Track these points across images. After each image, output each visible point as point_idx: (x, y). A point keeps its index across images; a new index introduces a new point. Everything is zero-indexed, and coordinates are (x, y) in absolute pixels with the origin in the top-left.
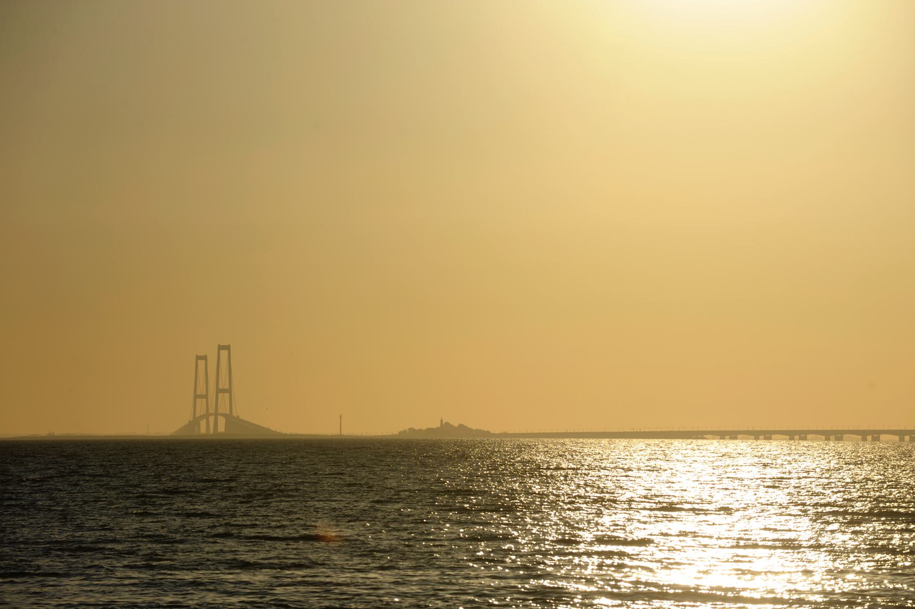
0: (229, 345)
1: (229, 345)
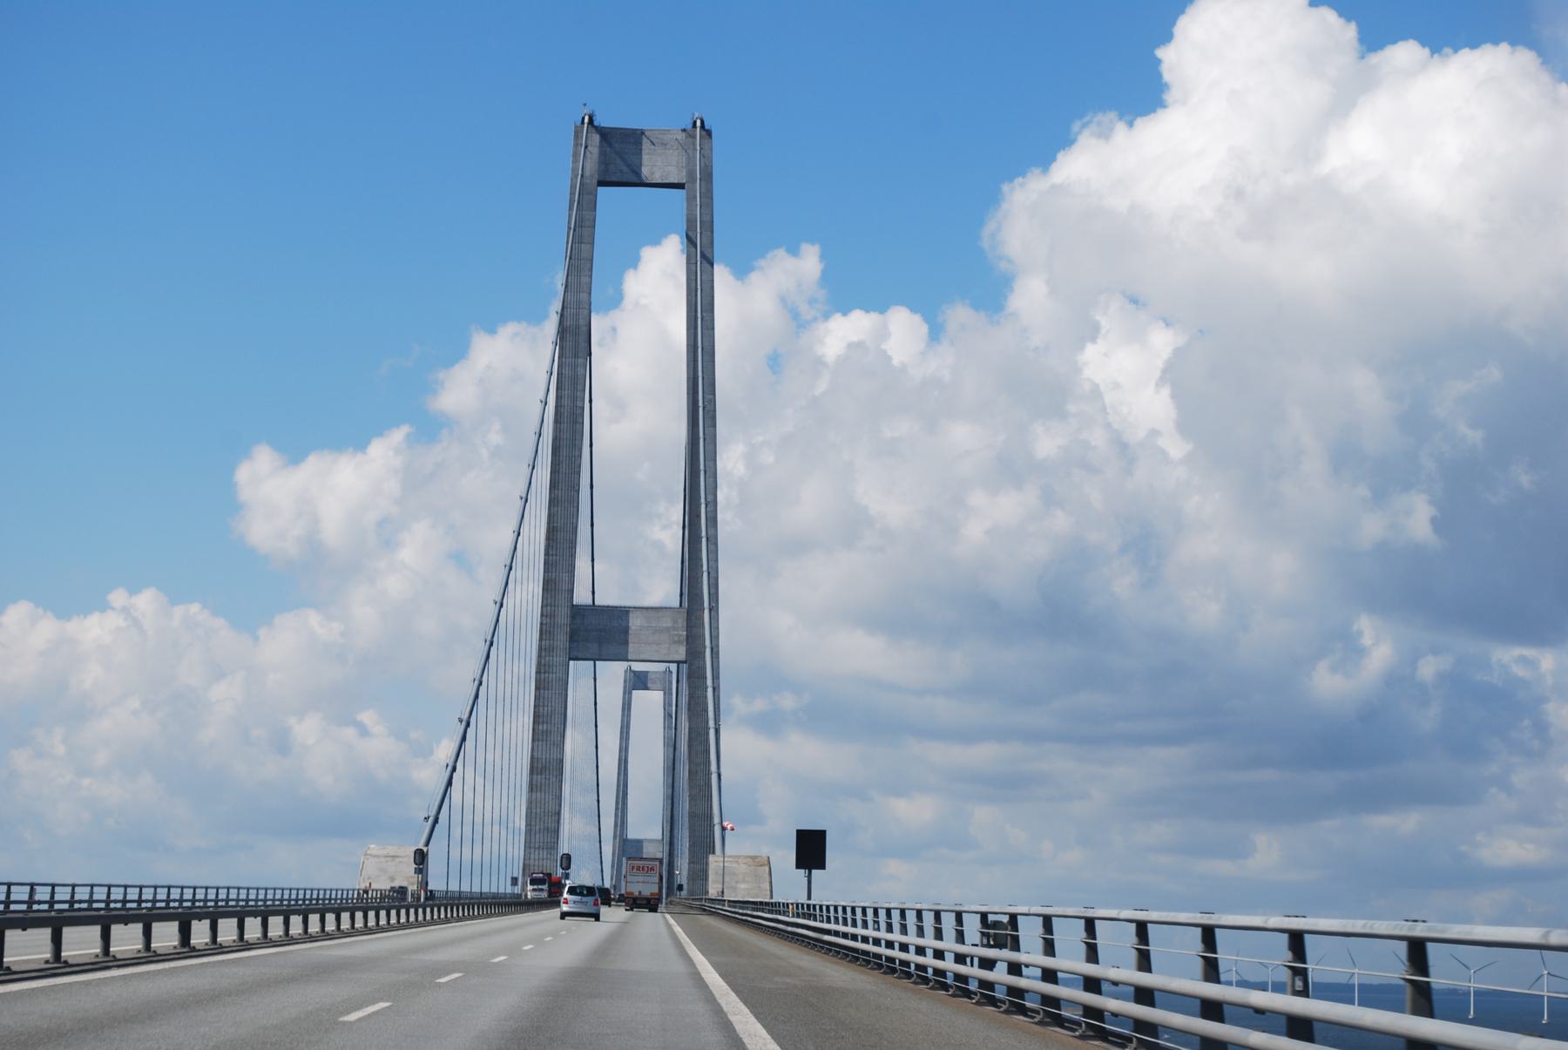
0: (1432, 56)
1: (1432, 56)
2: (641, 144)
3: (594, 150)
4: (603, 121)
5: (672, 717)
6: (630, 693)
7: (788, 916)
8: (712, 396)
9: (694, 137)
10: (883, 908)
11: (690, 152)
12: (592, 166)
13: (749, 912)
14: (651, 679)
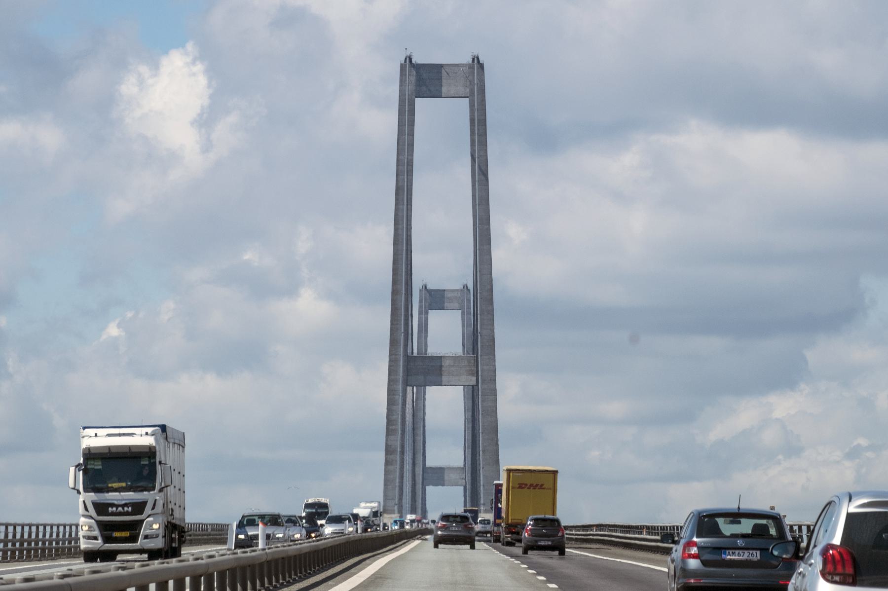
0: (476, 59)
1: (476, 59)
2: (441, 72)
3: (414, 73)
4: (417, 59)
5: (470, 301)
6: (427, 313)
7: (593, 531)
8: (488, 226)
9: (474, 69)
10: (804, 525)
11: (471, 78)
12: (410, 88)
13: (607, 533)
14: (448, 298)
